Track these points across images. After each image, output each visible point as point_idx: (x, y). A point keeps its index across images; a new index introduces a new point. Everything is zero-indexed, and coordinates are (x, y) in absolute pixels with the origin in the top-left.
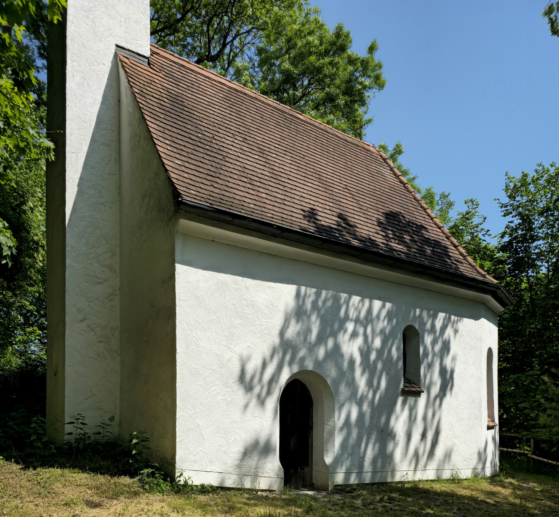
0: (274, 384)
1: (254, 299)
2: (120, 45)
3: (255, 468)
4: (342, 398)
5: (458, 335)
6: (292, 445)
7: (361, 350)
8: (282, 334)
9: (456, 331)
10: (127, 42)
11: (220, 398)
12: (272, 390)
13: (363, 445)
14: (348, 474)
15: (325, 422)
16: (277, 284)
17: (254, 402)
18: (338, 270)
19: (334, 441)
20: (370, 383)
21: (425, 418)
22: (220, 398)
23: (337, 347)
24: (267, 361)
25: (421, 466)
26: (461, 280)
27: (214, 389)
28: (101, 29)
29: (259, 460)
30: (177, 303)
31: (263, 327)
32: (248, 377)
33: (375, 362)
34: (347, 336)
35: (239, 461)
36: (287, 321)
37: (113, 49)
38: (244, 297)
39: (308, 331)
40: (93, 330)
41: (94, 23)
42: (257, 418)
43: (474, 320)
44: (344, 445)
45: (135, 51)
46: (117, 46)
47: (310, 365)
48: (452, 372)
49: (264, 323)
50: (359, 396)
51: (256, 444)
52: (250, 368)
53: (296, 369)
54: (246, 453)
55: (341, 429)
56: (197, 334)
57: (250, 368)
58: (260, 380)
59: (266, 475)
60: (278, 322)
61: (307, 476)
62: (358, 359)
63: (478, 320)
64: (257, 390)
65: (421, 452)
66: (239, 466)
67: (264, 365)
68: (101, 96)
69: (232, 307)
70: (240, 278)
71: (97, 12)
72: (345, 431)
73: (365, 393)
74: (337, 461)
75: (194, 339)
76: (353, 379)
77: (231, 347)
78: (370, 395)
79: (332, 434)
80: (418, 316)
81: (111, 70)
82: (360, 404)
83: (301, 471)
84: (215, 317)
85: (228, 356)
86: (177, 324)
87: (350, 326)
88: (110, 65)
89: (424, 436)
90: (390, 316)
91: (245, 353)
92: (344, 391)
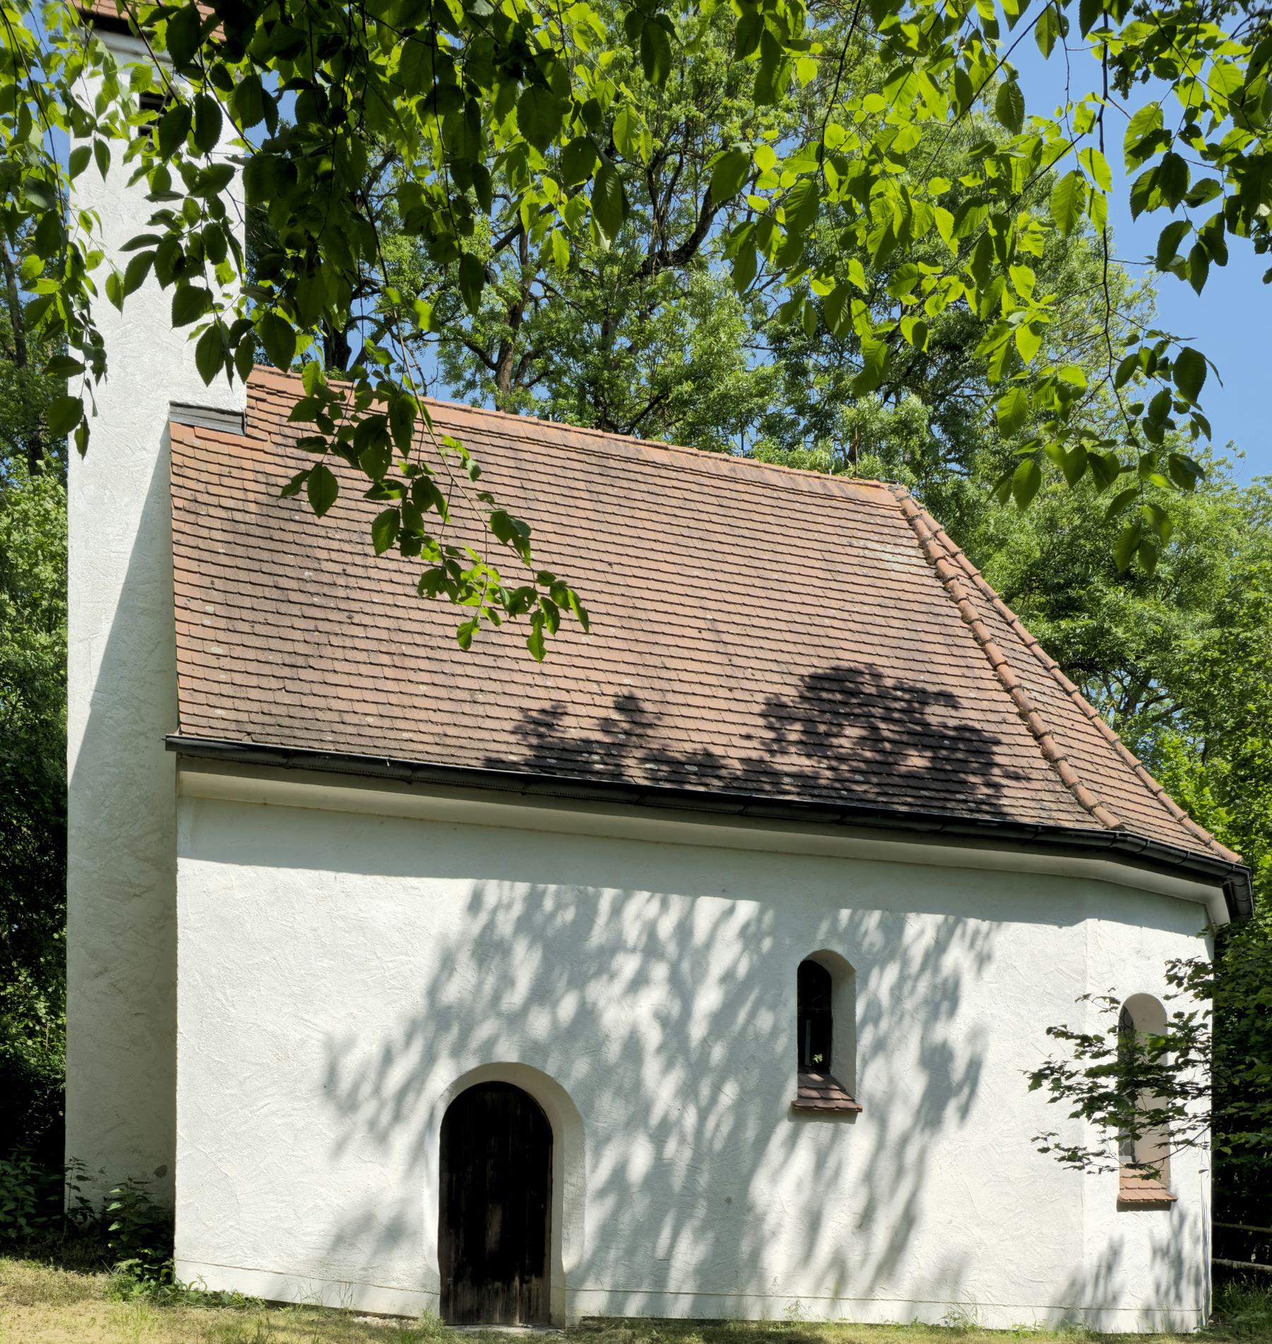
0: (410, 1098)
1: (364, 915)
2: (179, 401)
3: (364, 1269)
4: (602, 1124)
5: (990, 971)
6: (52, 1198)
7: (662, 1019)
8: (433, 991)
9: (983, 959)
10: (193, 393)
11: (280, 1122)
12: (405, 1110)
13: (666, 1233)
14: (619, 1294)
15: (566, 1176)
16: (425, 879)
17: (360, 1134)
18: (595, 836)
19: (583, 1219)
20: (688, 1092)
21: (869, 1177)
22: (280, 1122)
23: (587, 1015)
24: (394, 1051)
25: (852, 1291)
26: (972, 831)
27: (263, 1103)
28: (138, 378)
29: (375, 1253)
30: (180, 936)
31: (387, 974)
32: (345, 1084)
33: (706, 1042)
34: (618, 987)
35: (324, 1253)
36: (447, 963)
37: (164, 413)
38: (342, 913)
39: (507, 981)
40: (121, 992)
41: (124, 368)
42: (369, 1165)
43: (1055, 928)
44: (607, 1233)
45: (212, 406)
46: (174, 404)
47: (507, 1052)
48: (975, 1067)
49: (390, 965)
50: (655, 1118)
51: (365, 1223)
52: (351, 1064)
53: (471, 1063)
54: (341, 1240)
55: (601, 1193)
56: (225, 994)
57: (351, 1064)
58: (377, 1090)
59: (394, 1284)
60: (423, 962)
61: (538, 1297)
62: (653, 1036)
63: (1060, 927)
64: (368, 1109)
65: (854, 1258)
66: (324, 1263)
67: (388, 1058)
68: (140, 515)
69: (310, 935)
70: (331, 874)
71: (129, 346)
72: (610, 1201)
73: (674, 1114)
74: (591, 1267)
75: (217, 1004)
76: (638, 1084)
77: (306, 1017)
78: (690, 1119)
79: (578, 1204)
80: (846, 929)
81: (159, 457)
82: (659, 1137)
83: (521, 1285)
84: (267, 958)
85: (298, 1036)
86: (179, 976)
87: (628, 965)
88: (159, 446)
89: (865, 1220)
90: (749, 936)
91: (339, 1031)
92: (609, 1110)
